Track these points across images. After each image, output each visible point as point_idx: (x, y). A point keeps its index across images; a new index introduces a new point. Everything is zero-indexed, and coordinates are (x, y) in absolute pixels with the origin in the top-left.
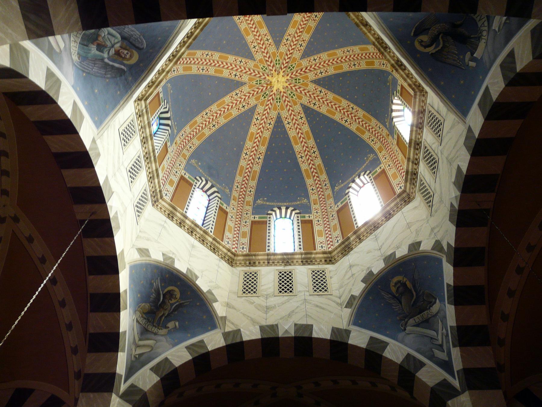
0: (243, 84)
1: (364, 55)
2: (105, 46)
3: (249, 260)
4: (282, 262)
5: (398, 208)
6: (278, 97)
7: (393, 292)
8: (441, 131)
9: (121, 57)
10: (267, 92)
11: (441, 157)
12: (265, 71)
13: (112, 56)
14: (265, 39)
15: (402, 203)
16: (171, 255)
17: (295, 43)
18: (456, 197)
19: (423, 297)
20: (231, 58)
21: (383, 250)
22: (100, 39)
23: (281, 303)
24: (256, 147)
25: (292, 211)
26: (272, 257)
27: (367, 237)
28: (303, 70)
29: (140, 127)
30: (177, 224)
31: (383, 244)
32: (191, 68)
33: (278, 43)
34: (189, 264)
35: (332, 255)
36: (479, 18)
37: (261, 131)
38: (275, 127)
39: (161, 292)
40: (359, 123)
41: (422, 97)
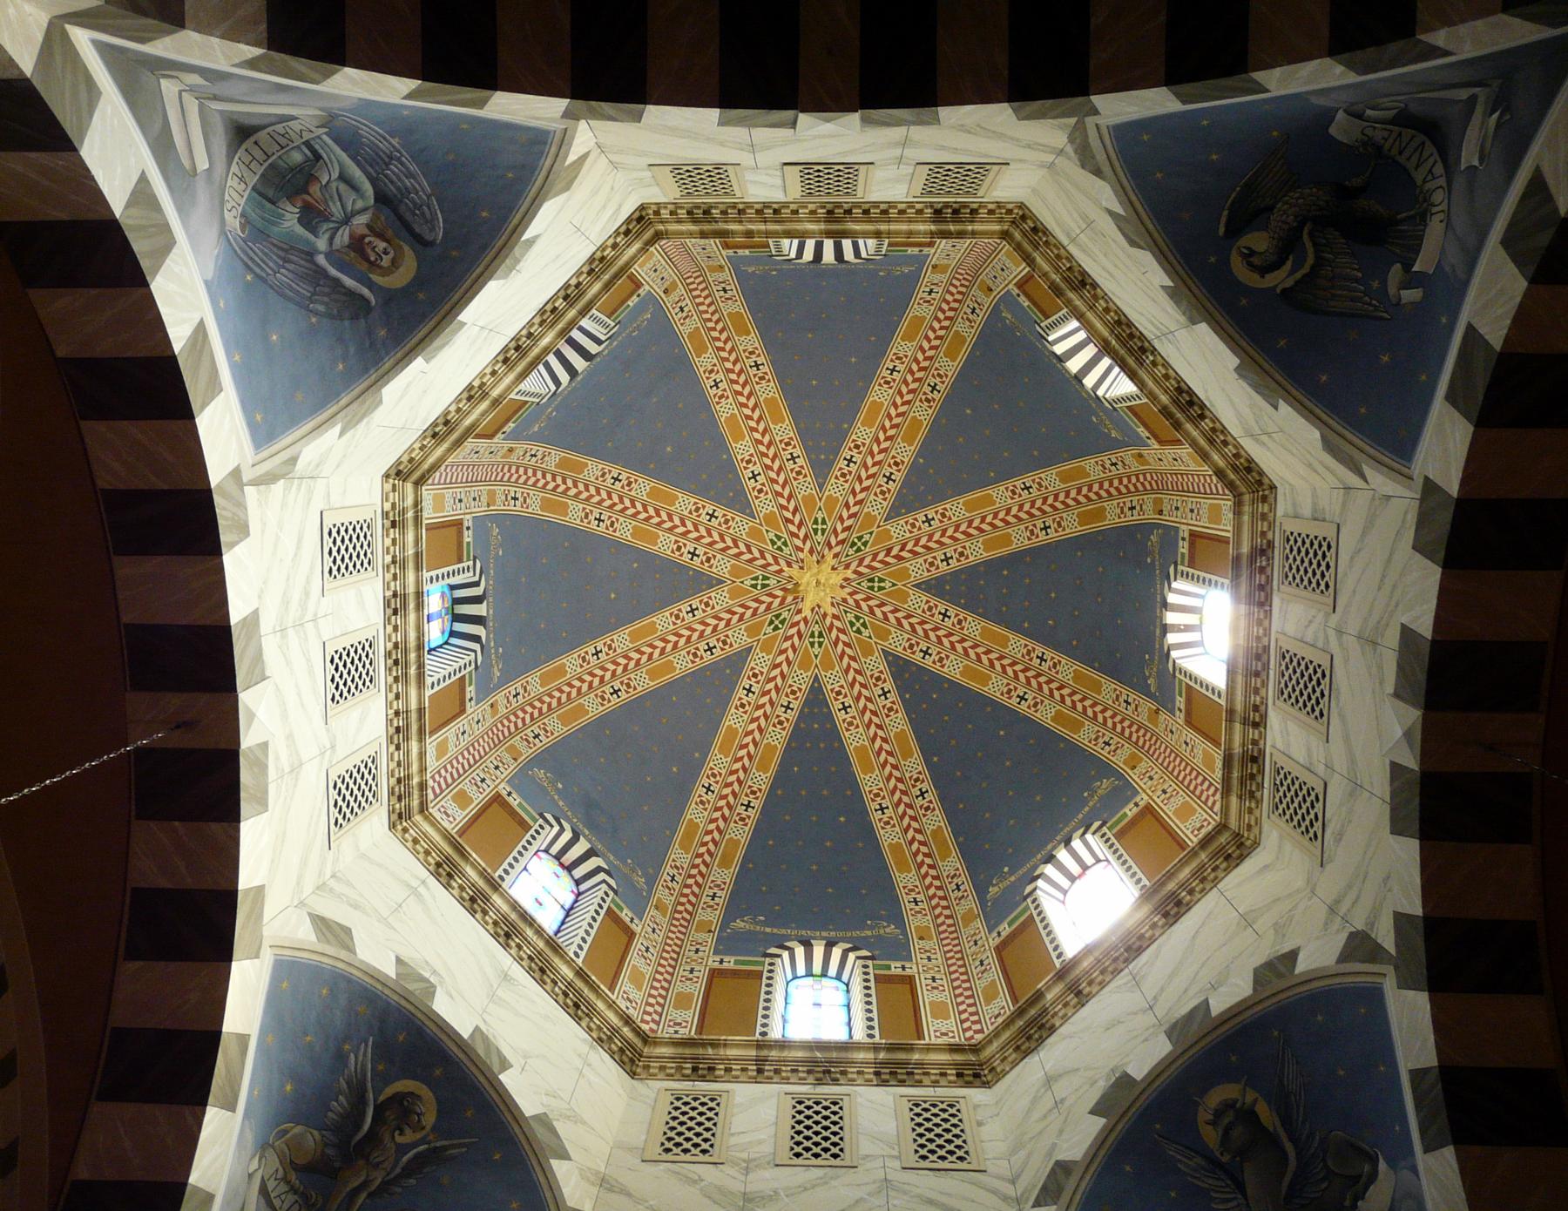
0: (715, 582)
1: (1073, 494)
2: (327, 218)
3: (695, 1058)
4: (809, 1072)
5: (1205, 880)
6: (816, 629)
7: (1211, 1146)
8: (1326, 698)
9: (367, 260)
10: (785, 615)
11: (1341, 644)
12: (782, 550)
13: (338, 250)
14: (786, 455)
15: (1217, 863)
16: (427, 975)
17: (873, 470)
18: (1408, 734)
19: (1324, 1160)
20: (684, 502)
21: (1160, 1011)
22: (315, 189)
23: (799, 1187)
24: (741, 774)
25: (845, 953)
26: (774, 1054)
27: (1103, 985)
28: (894, 552)
29: (388, 559)
30: (461, 900)
31: (1162, 990)
32: (566, 506)
33: (821, 470)
34: (484, 1021)
35: (982, 1057)
36: (1414, 159)
37: (754, 740)
38: (802, 716)
39: (371, 1096)
40: (1063, 700)
41: (1260, 505)
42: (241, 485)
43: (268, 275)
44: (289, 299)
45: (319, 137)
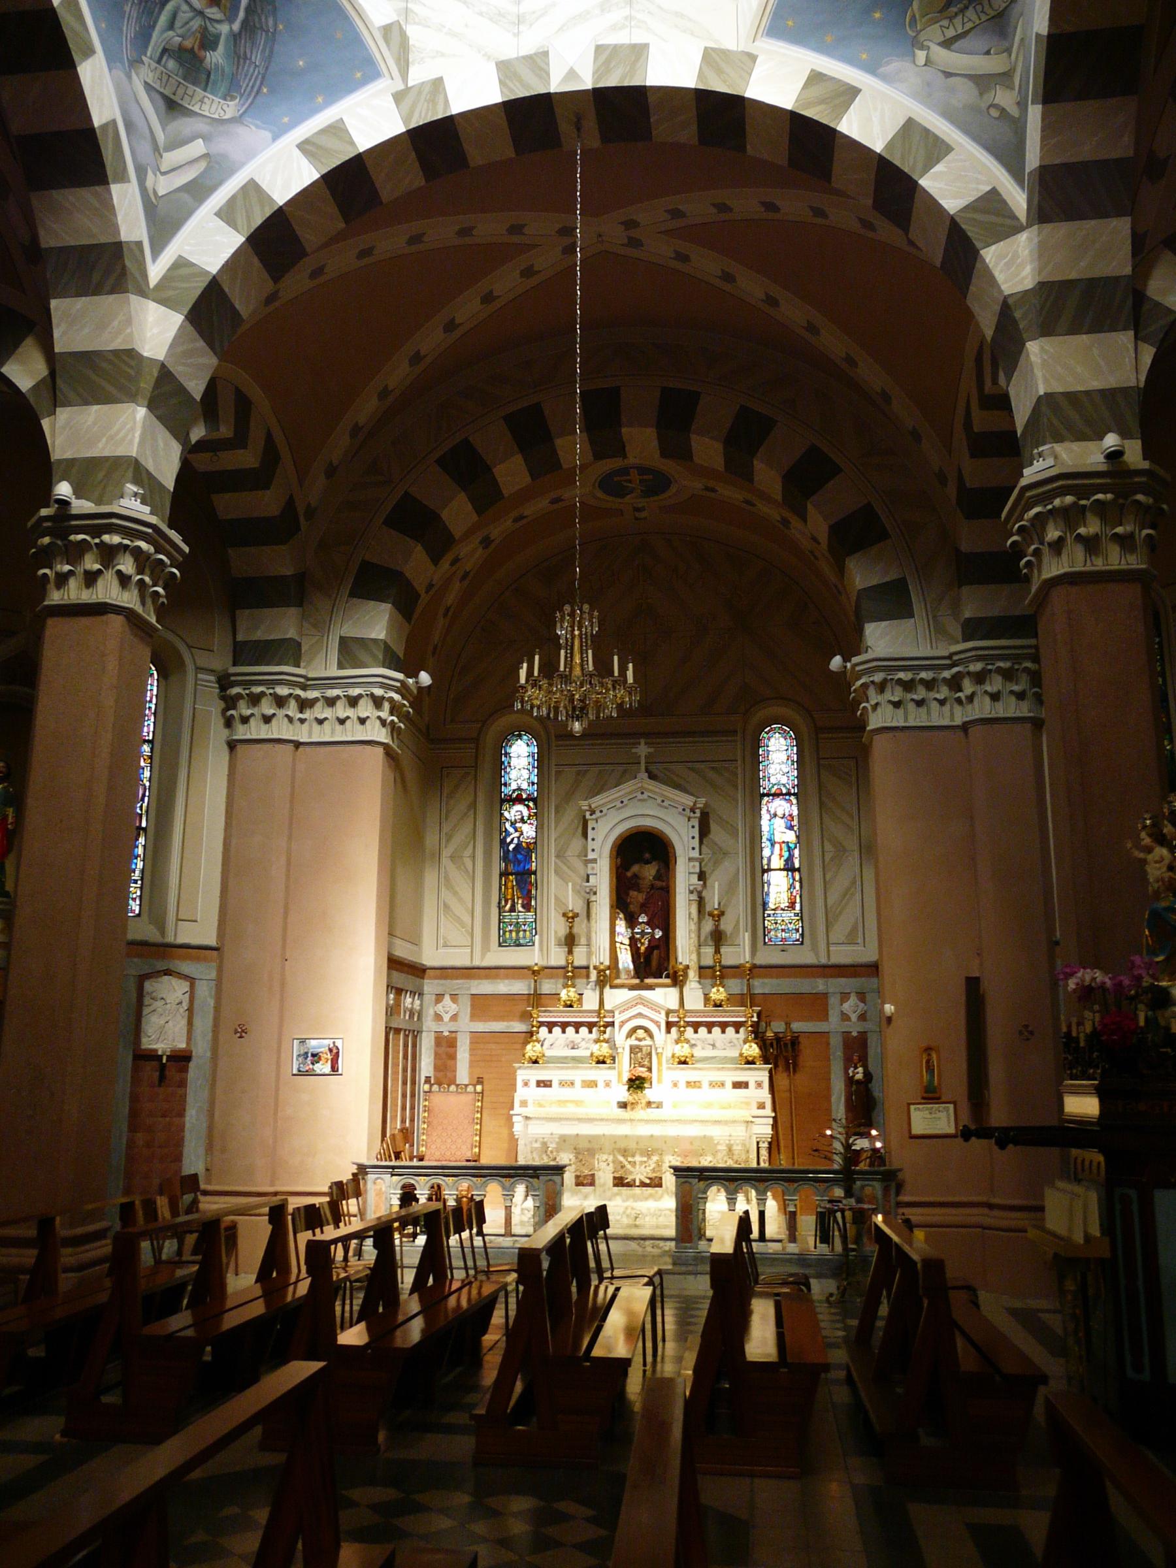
2: (204, 31)
22: (188, 44)
42: (408, 89)
43: (259, 72)
44: (271, 52)
45: (151, 58)
